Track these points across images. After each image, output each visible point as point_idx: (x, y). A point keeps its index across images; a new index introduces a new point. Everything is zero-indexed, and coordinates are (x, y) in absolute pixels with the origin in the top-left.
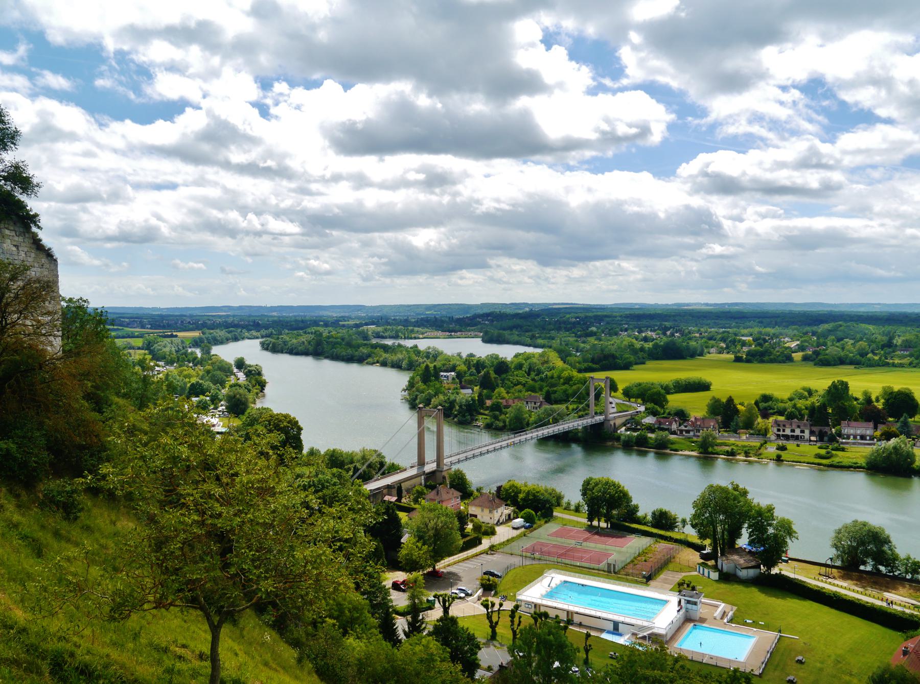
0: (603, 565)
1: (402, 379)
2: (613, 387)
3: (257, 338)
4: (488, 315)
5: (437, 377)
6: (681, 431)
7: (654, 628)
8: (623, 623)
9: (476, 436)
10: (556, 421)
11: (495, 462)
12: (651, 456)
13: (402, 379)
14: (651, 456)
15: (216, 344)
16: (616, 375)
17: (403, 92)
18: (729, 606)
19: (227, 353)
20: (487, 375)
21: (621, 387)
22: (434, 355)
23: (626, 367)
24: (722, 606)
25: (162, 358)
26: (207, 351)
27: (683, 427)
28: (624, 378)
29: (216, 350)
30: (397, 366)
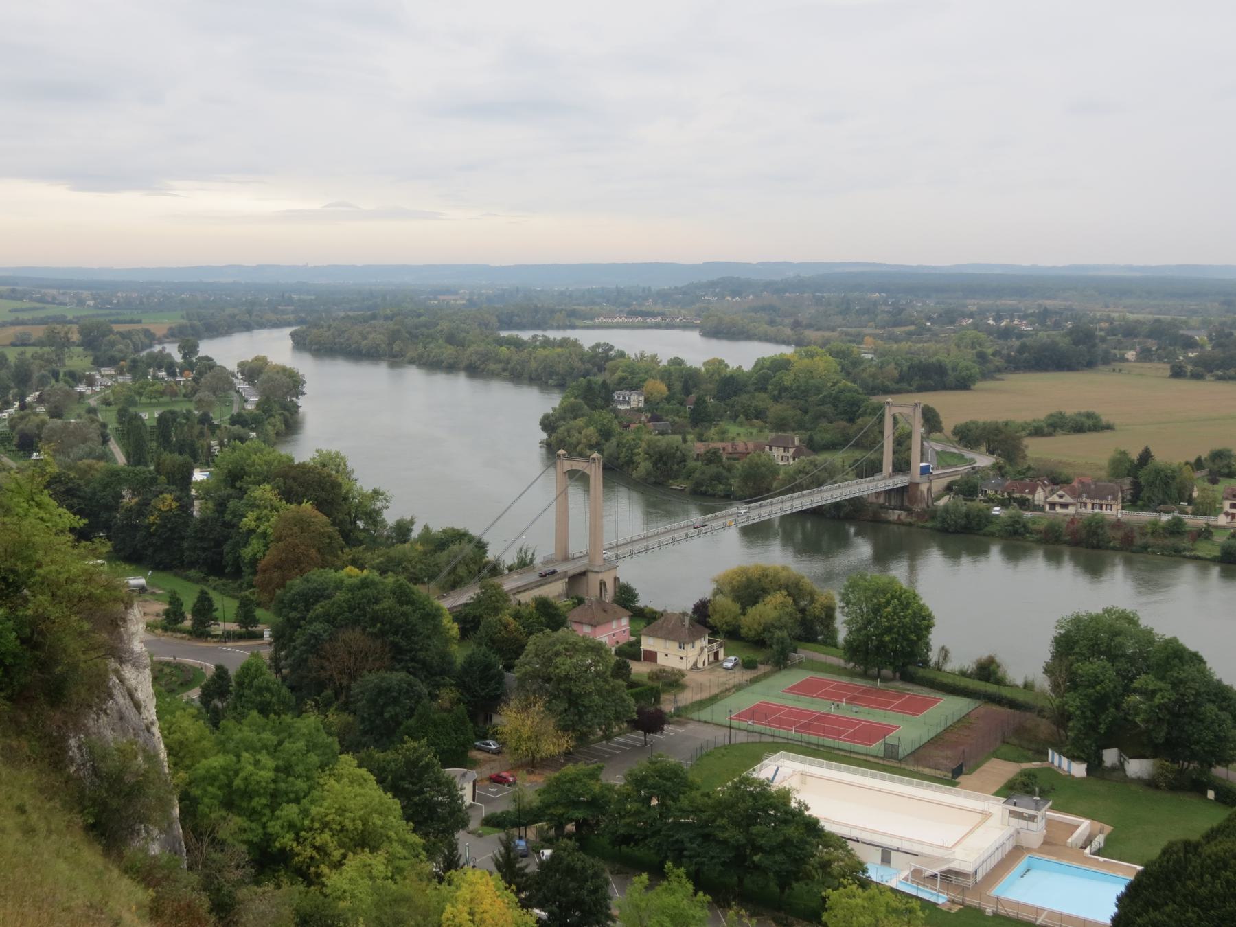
0: (877, 747)
1: (538, 403)
2: (931, 420)
3: (289, 324)
4: (713, 284)
5: (608, 400)
6: (1053, 506)
7: (953, 860)
8: (898, 850)
9: (807, 580)
10: (818, 483)
11: (693, 558)
12: (995, 551)
13: (538, 403)
14: (995, 551)
15: (211, 337)
16: (938, 400)
17: (150, 627)
18: (1098, 825)
19: (228, 352)
20: (700, 401)
21: (948, 423)
22: (602, 358)
23: (963, 384)
24: (1085, 825)
25: (112, 362)
26: (189, 349)
27: (1055, 498)
28: (955, 408)
29: (207, 348)
30: (518, 375)
